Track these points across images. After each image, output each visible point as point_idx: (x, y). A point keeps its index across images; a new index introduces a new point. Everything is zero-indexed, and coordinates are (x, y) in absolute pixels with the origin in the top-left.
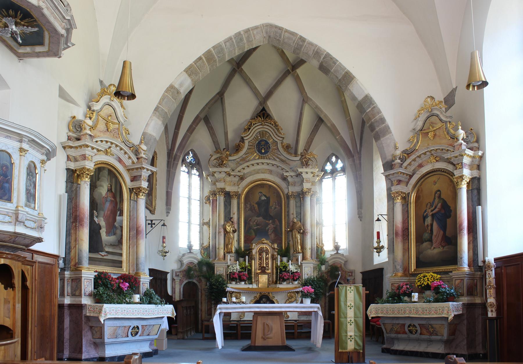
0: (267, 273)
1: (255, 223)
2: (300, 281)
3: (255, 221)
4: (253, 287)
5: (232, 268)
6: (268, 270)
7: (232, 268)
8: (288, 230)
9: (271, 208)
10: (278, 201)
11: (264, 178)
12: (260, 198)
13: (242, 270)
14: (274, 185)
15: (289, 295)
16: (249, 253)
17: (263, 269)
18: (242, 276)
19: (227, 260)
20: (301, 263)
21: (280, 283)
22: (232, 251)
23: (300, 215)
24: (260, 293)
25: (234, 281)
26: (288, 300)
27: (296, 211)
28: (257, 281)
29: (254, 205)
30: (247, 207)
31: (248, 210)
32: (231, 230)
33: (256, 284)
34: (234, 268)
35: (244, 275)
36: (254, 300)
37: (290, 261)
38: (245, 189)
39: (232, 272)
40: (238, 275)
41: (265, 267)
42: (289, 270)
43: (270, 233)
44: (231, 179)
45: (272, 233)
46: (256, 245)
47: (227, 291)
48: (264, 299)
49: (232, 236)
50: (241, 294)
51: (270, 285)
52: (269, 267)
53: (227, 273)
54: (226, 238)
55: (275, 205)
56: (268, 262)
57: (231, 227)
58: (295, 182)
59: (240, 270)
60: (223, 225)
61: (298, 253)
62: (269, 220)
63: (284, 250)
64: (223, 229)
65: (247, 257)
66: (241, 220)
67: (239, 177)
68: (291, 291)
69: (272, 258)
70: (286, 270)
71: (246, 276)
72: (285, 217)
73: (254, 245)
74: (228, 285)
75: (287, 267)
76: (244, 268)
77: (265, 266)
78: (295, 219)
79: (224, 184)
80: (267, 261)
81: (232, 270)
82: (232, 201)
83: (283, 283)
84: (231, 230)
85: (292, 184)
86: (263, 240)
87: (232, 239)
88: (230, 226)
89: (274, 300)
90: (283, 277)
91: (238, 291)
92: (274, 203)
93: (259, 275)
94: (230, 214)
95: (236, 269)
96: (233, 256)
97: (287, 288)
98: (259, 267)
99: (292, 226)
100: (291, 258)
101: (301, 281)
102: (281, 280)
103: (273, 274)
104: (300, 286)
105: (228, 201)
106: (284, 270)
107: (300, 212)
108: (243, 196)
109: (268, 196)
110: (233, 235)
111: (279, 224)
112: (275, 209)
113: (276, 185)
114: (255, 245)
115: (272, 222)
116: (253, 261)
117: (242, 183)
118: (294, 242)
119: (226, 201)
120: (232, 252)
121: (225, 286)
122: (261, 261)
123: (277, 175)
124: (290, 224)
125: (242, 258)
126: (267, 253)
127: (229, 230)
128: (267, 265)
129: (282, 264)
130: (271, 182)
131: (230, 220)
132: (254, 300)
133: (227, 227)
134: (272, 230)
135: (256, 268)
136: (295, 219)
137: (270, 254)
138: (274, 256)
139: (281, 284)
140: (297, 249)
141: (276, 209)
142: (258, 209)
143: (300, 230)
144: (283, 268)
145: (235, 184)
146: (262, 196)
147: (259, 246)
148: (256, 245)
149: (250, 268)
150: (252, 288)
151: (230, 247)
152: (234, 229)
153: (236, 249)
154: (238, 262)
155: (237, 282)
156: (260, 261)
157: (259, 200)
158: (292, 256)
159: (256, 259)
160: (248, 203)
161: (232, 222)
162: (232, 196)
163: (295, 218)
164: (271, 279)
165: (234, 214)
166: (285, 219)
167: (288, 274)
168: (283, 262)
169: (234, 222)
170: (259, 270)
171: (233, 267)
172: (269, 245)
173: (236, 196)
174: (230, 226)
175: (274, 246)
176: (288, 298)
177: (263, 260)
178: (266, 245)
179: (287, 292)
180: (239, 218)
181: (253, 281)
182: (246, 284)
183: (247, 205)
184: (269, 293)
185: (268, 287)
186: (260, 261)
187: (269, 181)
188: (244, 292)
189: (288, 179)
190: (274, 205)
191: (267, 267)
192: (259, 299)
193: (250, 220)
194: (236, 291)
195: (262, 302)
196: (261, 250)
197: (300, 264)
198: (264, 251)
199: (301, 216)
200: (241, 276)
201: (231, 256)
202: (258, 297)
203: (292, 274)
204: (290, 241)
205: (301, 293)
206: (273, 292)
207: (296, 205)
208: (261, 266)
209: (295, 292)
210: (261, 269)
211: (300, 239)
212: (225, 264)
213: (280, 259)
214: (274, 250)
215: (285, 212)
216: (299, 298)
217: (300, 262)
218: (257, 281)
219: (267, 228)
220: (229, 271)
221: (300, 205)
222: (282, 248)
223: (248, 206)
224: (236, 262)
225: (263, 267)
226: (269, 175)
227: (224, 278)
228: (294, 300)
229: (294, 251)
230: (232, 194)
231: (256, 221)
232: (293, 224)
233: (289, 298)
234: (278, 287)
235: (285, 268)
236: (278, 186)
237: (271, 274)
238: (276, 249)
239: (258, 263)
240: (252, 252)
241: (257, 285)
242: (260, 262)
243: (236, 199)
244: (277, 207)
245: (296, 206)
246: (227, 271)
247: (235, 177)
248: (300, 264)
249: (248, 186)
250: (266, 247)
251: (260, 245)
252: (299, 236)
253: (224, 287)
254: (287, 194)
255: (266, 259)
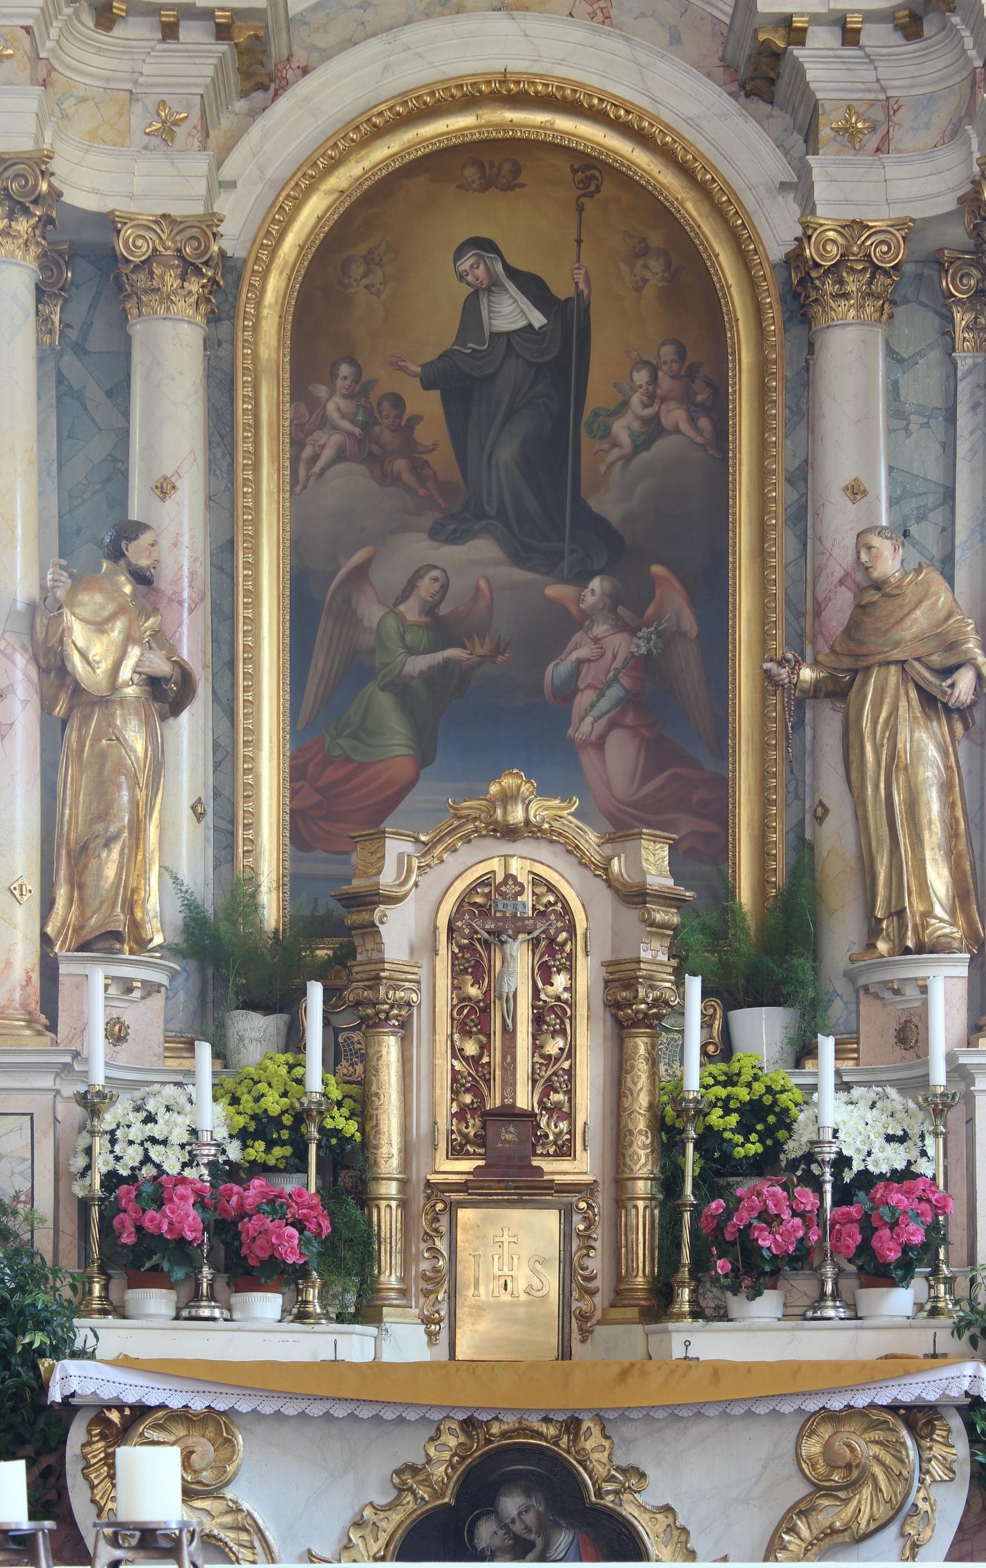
0: (551, 1187)
1: (411, 610)
2: (950, 1281)
3: (411, 585)
4: (388, 1356)
5: (138, 1131)
6: (565, 1150)
7: (138, 1131)
8: (807, 674)
9: (607, 432)
10: (682, 352)
11: (517, 65)
12: (471, 310)
13: (257, 1150)
14: (640, 158)
15: (812, 1447)
16: (346, 955)
17: (509, 1134)
18: (251, 1226)
19: (83, 1030)
20: (958, 1072)
21: (708, 1303)
22: (136, 926)
23: (937, 517)
24: (469, 1425)
25: (156, 1279)
26: (803, 1510)
27: (891, 469)
28: (433, 1280)
29: (398, 402)
30: (323, 422)
31: (340, 456)
32: (126, 673)
33: (427, 1321)
34: (157, 1130)
35: (274, 1203)
36: (392, 1506)
37: (827, 1045)
38: (297, 209)
39: (133, 1178)
40: (201, 1203)
41: (530, 1116)
42: (809, 1158)
43: (585, 728)
44: (126, 66)
45: (613, 725)
46: (427, 848)
47: (69, 1407)
48: (511, 1504)
49: (136, 740)
50: (229, 1442)
51: (586, 1334)
52: (570, 1116)
53: (79, 1190)
54: (68, 774)
55: (651, 398)
56: (570, 1052)
57: (129, 639)
58: (890, 107)
59: (234, 1152)
60: (32, 607)
61: (921, 948)
62: (581, 578)
63: (751, 923)
64: (35, 658)
65: (316, 991)
66: (254, 566)
67: (223, 32)
68: (837, 1404)
69: (614, 1006)
70: (778, 1147)
71: (299, 1225)
72: (762, 532)
73: (395, 847)
74: (82, 1337)
75: (786, 1122)
76: (276, 1121)
77: (524, 1099)
78: (884, 546)
79: (33, 105)
80: (554, 1046)
81: (133, 1156)
82: (137, 329)
83: (736, 1304)
84: (126, 673)
85: (848, 133)
86: (507, 798)
87: (134, 783)
88: (119, 626)
89: (629, 1510)
90: (745, 1233)
91: (198, 1405)
92: (641, 377)
93: (464, 1215)
94: (120, 501)
95: (179, 1135)
96: (150, 988)
97: (796, 1368)
98: (460, 1115)
99: (853, 628)
100: (837, 1011)
101: (962, 1285)
102: (723, 1267)
103: (621, 1201)
104: (946, 1343)
105: (96, 343)
106: (754, 1148)
107: (935, 474)
108: (275, 285)
109: (561, 289)
110: (151, 736)
111: (689, 623)
112: (643, 443)
113: (666, 154)
114: (407, 847)
115: (613, 601)
116: (390, 1048)
117: (256, 131)
118: (876, 817)
119: (80, 349)
120: (142, 944)
121: (38, 1339)
122: (485, 1047)
123: (675, 39)
124: (827, 614)
125: (266, 1008)
126: (553, 946)
127: (104, 667)
128: (550, 1088)
129: (731, 1081)
130: (598, 116)
131: (117, 554)
132: (392, 1506)
133: (79, 633)
134: (614, 693)
135: (421, 1125)
136: (884, 546)
137: (583, 966)
138: (630, 983)
139: (723, 1315)
140: (914, 906)
141: (663, 446)
142: (446, 448)
143: (948, 671)
144: (744, 1129)
145: (167, 131)
146: (493, 285)
147: (453, 863)
148: (427, 848)
149: (351, 1128)
150: (377, 1367)
151: (110, 872)
152: (159, 665)
153: (191, 906)
154: (204, 1050)
155: (197, 1296)
156: (471, 1048)
157: (461, 338)
158: (840, 985)
159: (420, 1021)
160: (334, 376)
161: (142, 578)
162: (141, 279)
163: (881, 531)
164: (596, 1263)
165: (164, 489)
166: (762, 555)
167: (808, 1199)
168: (743, 1061)
169: (164, 583)
170: (456, 1151)
171: (150, 1119)
172: (573, 850)
173: (188, 268)
174: (119, 626)
175: (635, 861)
176: (805, 1489)
177: (509, 1034)
178: (542, 851)
179: (787, 1408)
180: (230, 546)
181: (390, 1278)
182: (302, 1317)
183: (321, 391)
184: (572, 1425)
185: (565, 1353)
186: (471, 1048)
187: (572, 107)
188: (268, 1408)
189: (799, 71)
190: (635, 400)
191: (554, 1110)
192: (459, 1496)
193: (361, 573)
194: (176, 1403)
195: (486, 1532)
196: (484, 911)
197: (939, 1076)
198: (519, 926)
199: (948, 529)
200: (243, 1214)
201: (127, 986)
202: (439, 1471)
203: (843, 1195)
204: (821, 814)
205: (956, 1423)
206: (624, 1415)
207: (893, 391)
208: (477, 1109)
209: (893, 1408)
210: (481, 1140)
211: (946, 788)
212: (47, 1081)
213: (706, 1024)
214: (631, 915)
215: (762, 476)
216: (937, 1493)
217: (951, 1058)
218: (433, 1280)
219: (556, 671)
220: (102, 1164)
221: (936, 400)
222: (731, 892)
223: (335, 406)
224: (186, 1064)
225: (509, 1114)
226: (577, 33)
227: (43, 1242)
228: (882, 1512)
229: (873, 931)
230: (143, 250)
231: (426, 587)
232: (862, 608)
233: (821, 1489)
234: (678, 1352)
235: (770, 1132)
236: (684, 170)
237: (602, 1200)
238: (665, 899)
239: (445, 1063)
240: (371, 929)
241: (432, 1337)
242: (474, 1061)
243: (182, 307)
244: (674, 415)
245: (897, 412)
246: (81, 1162)
247: (170, 32)
248: (939, 1076)
249: (335, 164)
250: (537, 880)
251: (466, 854)
252: (932, 752)
253: (33, 1355)
254: (795, 258)
255: (538, 1020)
